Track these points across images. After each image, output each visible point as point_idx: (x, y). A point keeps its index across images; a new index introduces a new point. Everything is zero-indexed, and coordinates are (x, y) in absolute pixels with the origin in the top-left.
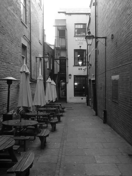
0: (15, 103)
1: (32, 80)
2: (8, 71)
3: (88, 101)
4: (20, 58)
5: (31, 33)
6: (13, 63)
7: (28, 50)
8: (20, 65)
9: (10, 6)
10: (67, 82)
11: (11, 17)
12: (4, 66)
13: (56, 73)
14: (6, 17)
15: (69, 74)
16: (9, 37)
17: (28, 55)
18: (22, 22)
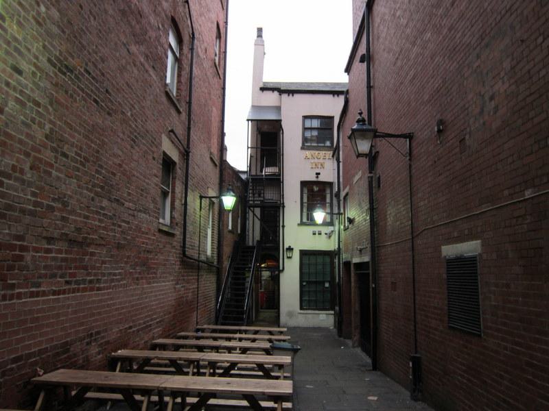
0: (131, 328)
1: (185, 258)
2: (113, 227)
3: (339, 323)
4: (155, 192)
5: (189, 129)
6: (131, 204)
7: (179, 172)
8: (155, 212)
9: (139, 44)
10: (281, 268)
11: (136, 71)
12: (102, 208)
13: (251, 244)
14: (122, 69)
15: (286, 246)
16: (124, 125)
17: (179, 188)
18: (167, 94)
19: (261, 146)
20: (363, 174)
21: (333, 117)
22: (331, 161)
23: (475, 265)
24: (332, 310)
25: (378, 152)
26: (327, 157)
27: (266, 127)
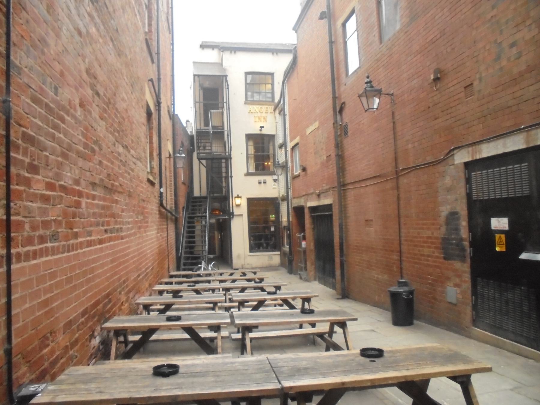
20: (321, 124)
22: (273, 115)
23: (189, 225)
24: (278, 251)
25: (344, 103)
26: (269, 111)
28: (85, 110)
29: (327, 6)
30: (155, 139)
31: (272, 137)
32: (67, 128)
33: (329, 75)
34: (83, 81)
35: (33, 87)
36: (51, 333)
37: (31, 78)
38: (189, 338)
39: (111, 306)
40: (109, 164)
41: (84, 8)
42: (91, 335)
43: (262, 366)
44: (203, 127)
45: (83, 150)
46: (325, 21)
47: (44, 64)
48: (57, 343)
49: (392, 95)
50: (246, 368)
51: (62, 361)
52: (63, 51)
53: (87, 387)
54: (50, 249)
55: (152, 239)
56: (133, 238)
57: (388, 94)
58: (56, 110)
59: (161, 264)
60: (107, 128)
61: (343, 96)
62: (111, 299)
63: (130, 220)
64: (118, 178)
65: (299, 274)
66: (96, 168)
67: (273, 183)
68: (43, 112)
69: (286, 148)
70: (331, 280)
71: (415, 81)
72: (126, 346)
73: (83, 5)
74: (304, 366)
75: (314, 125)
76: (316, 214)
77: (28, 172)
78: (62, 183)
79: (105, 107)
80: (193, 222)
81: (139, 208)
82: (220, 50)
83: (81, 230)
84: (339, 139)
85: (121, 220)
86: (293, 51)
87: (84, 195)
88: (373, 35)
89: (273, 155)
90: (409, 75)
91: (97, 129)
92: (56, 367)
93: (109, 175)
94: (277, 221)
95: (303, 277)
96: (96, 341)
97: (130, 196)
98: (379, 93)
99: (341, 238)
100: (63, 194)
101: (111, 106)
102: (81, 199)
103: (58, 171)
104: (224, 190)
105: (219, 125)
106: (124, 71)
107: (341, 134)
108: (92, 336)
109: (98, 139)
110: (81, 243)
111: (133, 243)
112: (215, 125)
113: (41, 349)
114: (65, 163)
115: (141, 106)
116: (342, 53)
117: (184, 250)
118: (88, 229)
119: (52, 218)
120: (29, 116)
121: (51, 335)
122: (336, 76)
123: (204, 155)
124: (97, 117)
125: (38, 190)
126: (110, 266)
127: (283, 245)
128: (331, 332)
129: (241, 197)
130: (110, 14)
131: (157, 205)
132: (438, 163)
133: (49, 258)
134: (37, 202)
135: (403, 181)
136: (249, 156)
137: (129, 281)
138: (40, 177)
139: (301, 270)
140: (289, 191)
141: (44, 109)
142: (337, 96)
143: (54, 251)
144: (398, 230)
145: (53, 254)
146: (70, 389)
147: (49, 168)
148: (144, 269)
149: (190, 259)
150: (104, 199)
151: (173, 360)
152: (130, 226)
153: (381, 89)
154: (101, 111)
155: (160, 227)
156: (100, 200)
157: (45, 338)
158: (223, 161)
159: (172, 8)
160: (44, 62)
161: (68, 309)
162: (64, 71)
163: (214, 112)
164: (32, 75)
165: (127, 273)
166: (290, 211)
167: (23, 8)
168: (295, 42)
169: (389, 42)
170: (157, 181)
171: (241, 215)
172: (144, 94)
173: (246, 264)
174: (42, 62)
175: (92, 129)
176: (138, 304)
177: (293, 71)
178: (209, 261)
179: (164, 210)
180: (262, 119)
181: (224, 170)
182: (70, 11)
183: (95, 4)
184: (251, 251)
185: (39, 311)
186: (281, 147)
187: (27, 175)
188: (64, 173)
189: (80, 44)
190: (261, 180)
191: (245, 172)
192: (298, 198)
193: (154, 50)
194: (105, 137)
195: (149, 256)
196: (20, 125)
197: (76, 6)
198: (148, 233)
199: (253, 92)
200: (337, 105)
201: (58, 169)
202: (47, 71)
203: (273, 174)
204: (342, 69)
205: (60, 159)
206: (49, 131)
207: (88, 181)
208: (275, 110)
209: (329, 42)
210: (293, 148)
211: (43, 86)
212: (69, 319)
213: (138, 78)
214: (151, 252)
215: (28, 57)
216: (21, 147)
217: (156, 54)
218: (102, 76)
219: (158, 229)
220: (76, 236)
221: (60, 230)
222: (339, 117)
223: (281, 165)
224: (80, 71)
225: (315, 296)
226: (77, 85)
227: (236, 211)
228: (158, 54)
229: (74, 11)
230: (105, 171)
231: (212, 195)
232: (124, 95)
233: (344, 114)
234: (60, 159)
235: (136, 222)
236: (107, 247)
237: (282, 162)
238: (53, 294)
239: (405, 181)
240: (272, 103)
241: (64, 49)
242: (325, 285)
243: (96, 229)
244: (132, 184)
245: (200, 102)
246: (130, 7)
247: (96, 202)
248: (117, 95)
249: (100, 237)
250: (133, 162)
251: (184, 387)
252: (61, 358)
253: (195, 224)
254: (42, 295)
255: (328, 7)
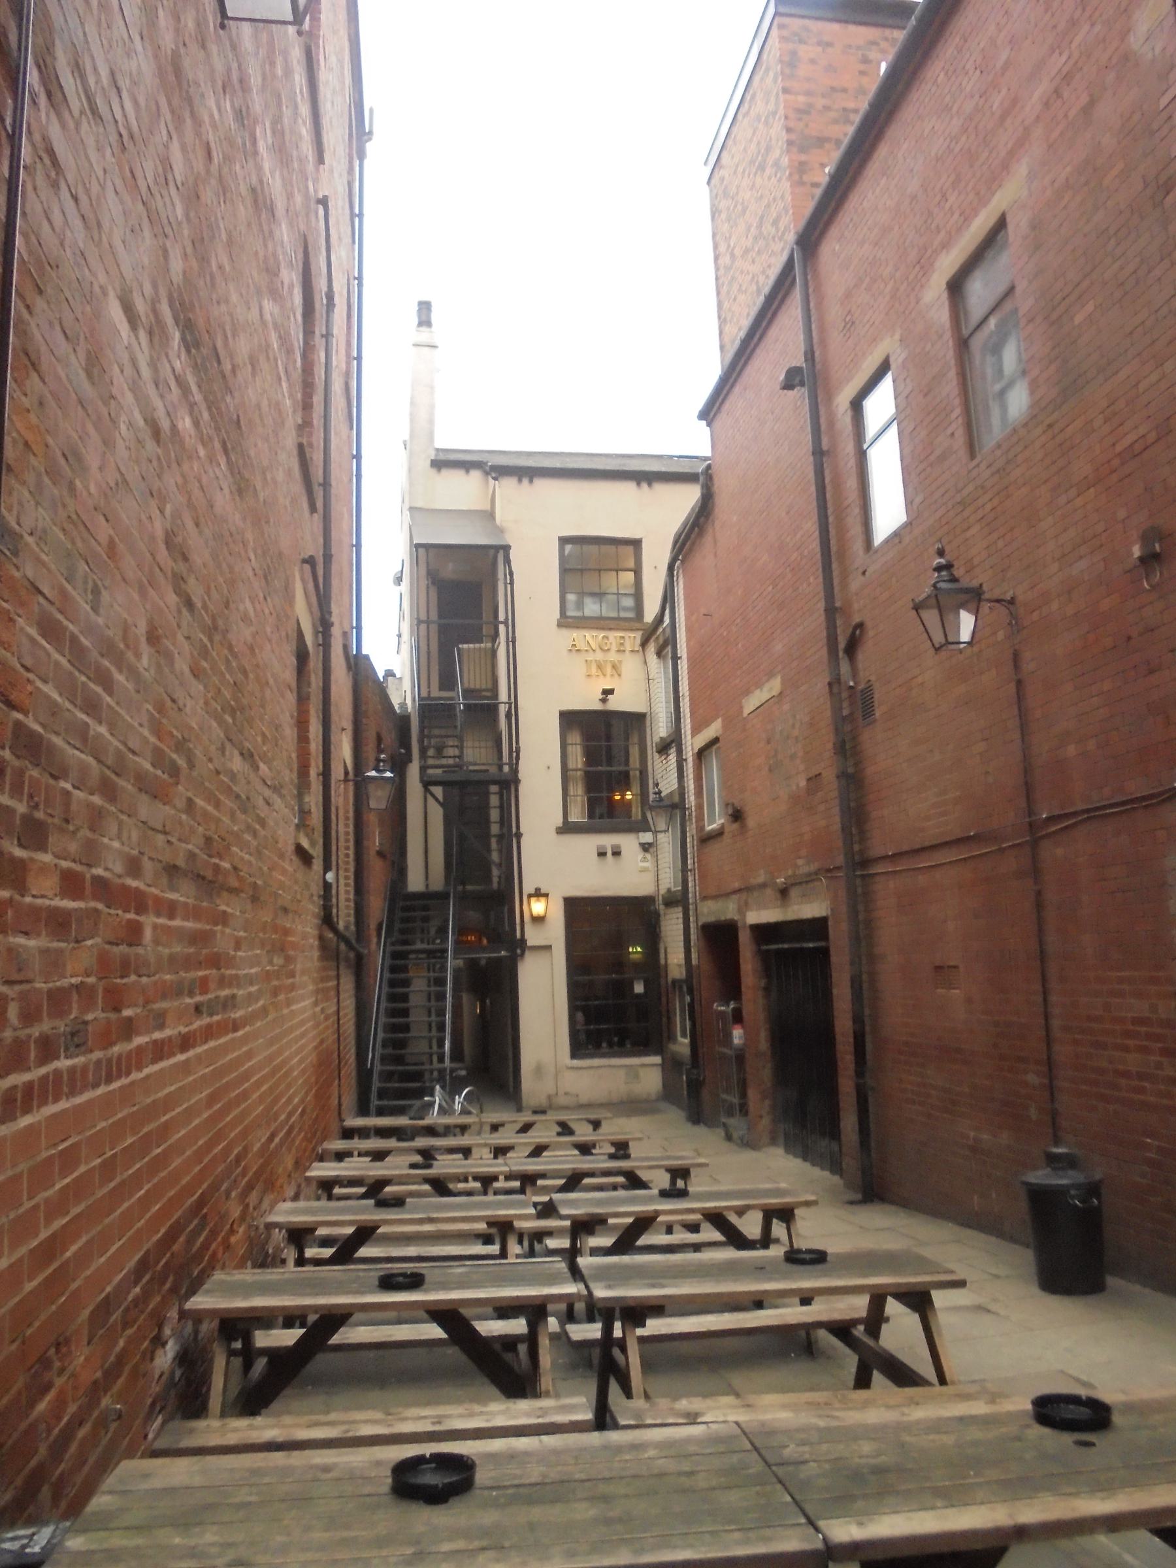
19: (440, 616)
20: (790, 684)
21: (636, 544)
22: (638, 658)
24: (656, 1053)
26: (628, 647)
27: (450, 566)
28: (158, 652)
29: (806, 353)
30: (315, 729)
31: (636, 721)
32: (117, 708)
33: (815, 545)
34: (157, 570)
35: (46, 591)
36: (58, 1345)
37: (44, 564)
38: (440, 1340)
39: (206, 1239)
40: (210, 808)
41: (169, 361)
42: (154, 1338)
43: (735, 1458)
44: (436, 693)
45: (151, 769)
46: (799, 395)
47: (73, 523)
48: (73, 1375)
49: (1012, 601)
50: (686, 1467)
51: (81, 1433)
52: (117, 484)
53: (192, 1542)
54: (65, 1078)
55: (303, 1023)
56: (259, 1024)
57: (998, 601)
58: (94, 654)
59: (322, 1095)
60: (206, 703)
61: (856, 606)
62: (205, 1215)
63: (253, 971)
64: (228, 848)
65: (724, 1125)
66: (180, 823)
67: (641, 855)
68: (64, 662)
69: (680, 752)
70: (824, 1144)
71: (1082, 565)
72: (248, 1366)
73: (167, 356)
74: (873, 1461)
75: (766, 688)
76: (774, 947)
77: (20, 845)
78: (99, 871)
79: (205, 640)
80: (405, 969)
81: (276, 933)
82: (487, 473)
83: (139, 1010)
84: (848, 728)
85: (234, 972)
86: (701, 478)
87: (150, 903)
88: (949, 431)
89: (641, 773)
90: (1062, 546)
91: (185, 706)
92: (67, 1456)
93: (208, 840)
94: (653, 965)
95: (735, 1135)
96: (165, 1358)
97: (255, 899)
98: (973, 598)
99: (858, 1019)
100: (100, 906)
101: (217, 638)
102: (141, 919)
103: (89, 834)
104: (495, 872)
105: (484, 687)
106: (249, 536)
107: (851, 714)
108: (159, 1342)
109: (186, 736)
110: (140, 1050)
111: (261, 1040)
112: (472, 686)
113: (32, 1404)
114: (108, 811)
115: (284, 634)
116: (852, 483)
117: (379, 1050)
118: (156, 1006)
119: (73, 980)
120: (31, 676)
121: (58, 1351)
122: (834, 549)
123: (439, 771)
124: (187, 670)
125: (43, 896)
126: (205, 1115)
127: (672, 1037)
128: (876, 1319)
129: (546, 895)
130: (224, 377)
131: (317, 921)
132: (1164, 801)
133: (63, 1105)
134: (39, 935)
135: (1053, 853)
136: (570, 773)
137: (250, 1155)
138: (46, 858)
139: (730, 1113)
140: (690, 879)
141: (67, 651)
142: (838, 604)
143: (75, 1082)
144: (1039, 999)
145: (72, 1093)
146: (138, 1547)
147: (71, 828)
148: (283, 1117)
149: (396, 1077)
150: (195, 913)
151: (406, 1419)
152: (253, 989)
153: (981, 585)
154: (195, 653)
155: (321, 986)
156: (186, 918)
157: (44, 1363)
158: (494, 788)
159: (359, 358)
160: (74, 517)
161: (103, 1259)
162: (117, 539)
163: (469, 649)
164: (44, 557)
165: (245, 1134)
166: (693, 937)
167: (33, 364)
168: (708, 453)
169: (998, 453)
170: (317, 852)
171: (548, 948)
172: (290, 599)
173: (561, 1092)
174: (69, 517)
175: (174, 706)
176: (270, 1226)
177: (701, 533)
178: (453, 1090)
179: (331, 935)
180: (609, 670)
181: (494, 815)
182: (138, 372)
183: (193, 351)
184: (574, 1055)
185: (30, 1279)
186: (663, 748)
187: (19, 853)
188: (106, 840)
189: (155, 463)
190: (604, 847)
191: (559, 821)
192: (715, 897)
193: (318, 474)
194: (201, 728)
195: (295, 1073)
196: (11, 705)
197: (151, 357)
198: (294, 1007)
199: (582, 594)
200: (839, 631)
201: (92, 829)
202: (80, 544)
203: (643, 826)
204: (856, 530)
205: (96, 800)
206: (75, 716)
207: (160, 861)
208: (644, 644)
209: (813, 453)
210: (701, 754)
211: (69, 587)
212: (103, 1295)
213: (280, 554)
214: (301, 1062)
215: (37, 503)
216: (9, 771)
217: (320, 485)
218: (200, 555)
219: (317, 991)
220: (128, 1029)
221: (89, 1017)
222: (845, 667)
223: (667, 802)
224: (153, 538)
225: (808, 1204)
226: (144, 580)
227: (533, 937)
228: (326, 485)
229: (146, 372)
230: (201, 829)
231: (460, 888)
232: (248, 604)
233: (860, 656)
234: (96, 800)
235: (268, 976)
236: (199, 1058)
237: (669, 791)
238: (67, 1219)
239: (1060, 851)
240: (638, 625)
241: (118, 476)
242: (805, 1159)
243: (176, 1004)
244: (260, 864)
245: (428, 622)
246: (268, 358)
247: (177, 923)
248: (232, 606)
249: (184, 1030)
250: (264, 799)
251: (507, 1544)
252: (80, 1424)
253: (411, 974)
254: (42, 1225)
255: (810, 355)
